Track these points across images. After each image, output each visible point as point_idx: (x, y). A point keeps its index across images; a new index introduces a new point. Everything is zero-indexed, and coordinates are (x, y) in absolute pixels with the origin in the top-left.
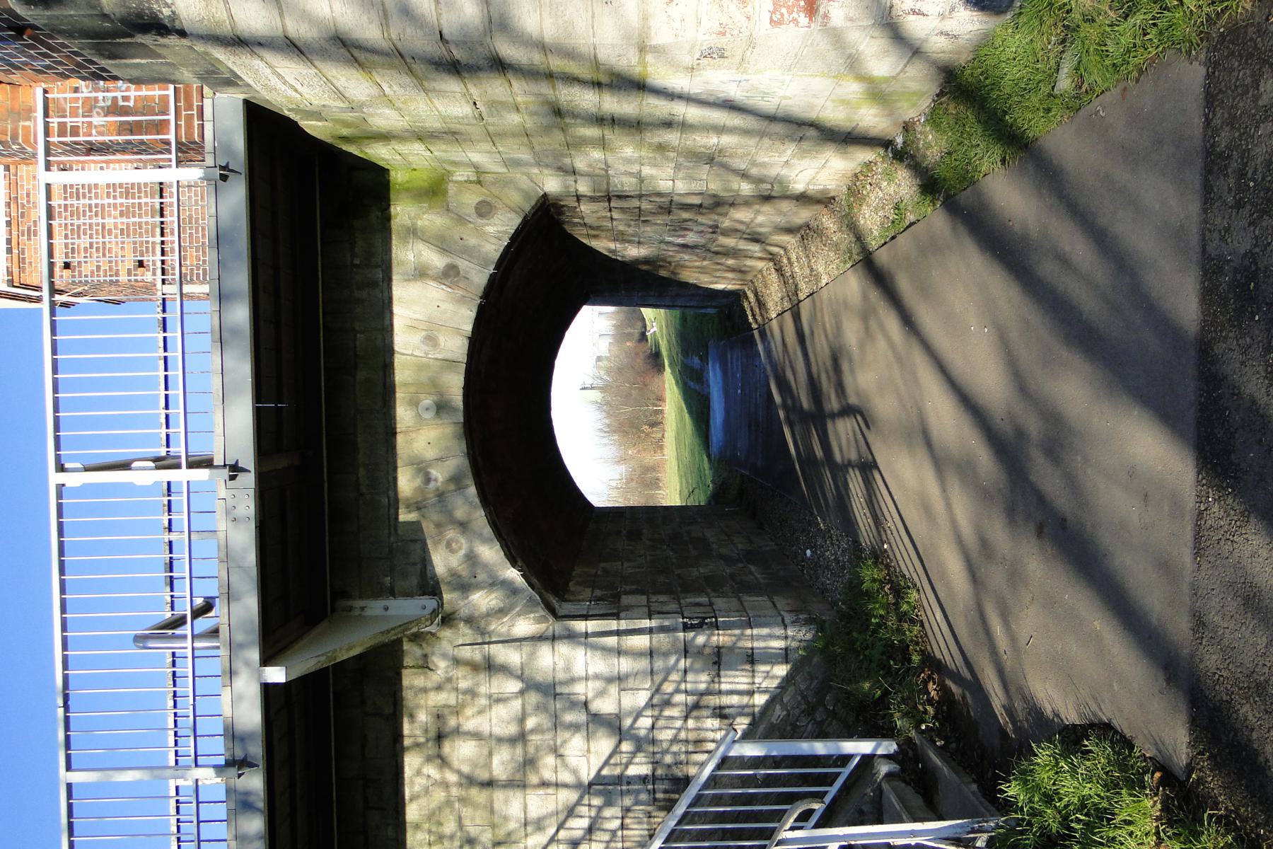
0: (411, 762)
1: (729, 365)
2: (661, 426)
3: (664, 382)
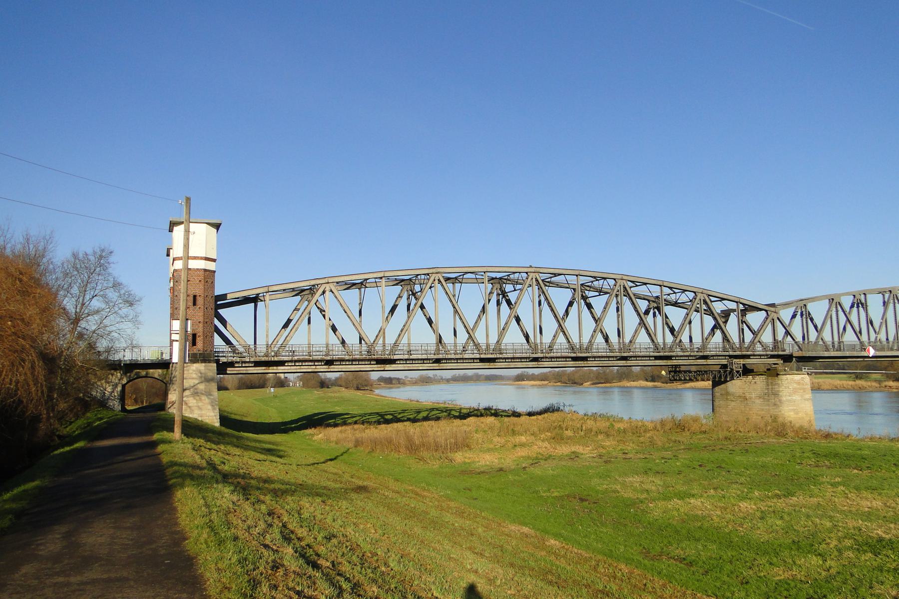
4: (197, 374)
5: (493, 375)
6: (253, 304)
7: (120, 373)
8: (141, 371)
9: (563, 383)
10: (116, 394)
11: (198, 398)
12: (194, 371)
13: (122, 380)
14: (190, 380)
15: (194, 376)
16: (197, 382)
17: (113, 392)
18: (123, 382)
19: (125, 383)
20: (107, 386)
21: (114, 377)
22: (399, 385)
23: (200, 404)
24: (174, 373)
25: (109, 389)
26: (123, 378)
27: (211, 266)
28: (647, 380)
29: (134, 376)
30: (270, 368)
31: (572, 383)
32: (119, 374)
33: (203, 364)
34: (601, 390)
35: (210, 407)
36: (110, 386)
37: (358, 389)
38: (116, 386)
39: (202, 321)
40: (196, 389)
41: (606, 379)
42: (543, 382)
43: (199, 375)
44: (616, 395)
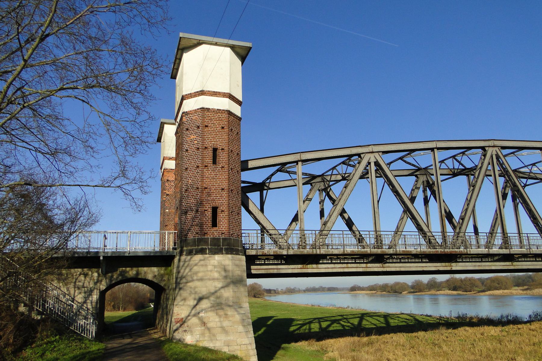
0: (80, 270)
1: (512, 180)
2: (113, 310)
3: (131, 311)
4: (219, 272)
5: (332, 287)
6: (259, 192)
7: (97, 272)
8: (128, 269)
9: (388, 292)
10: (89, 306)
11: (221, 312)
12: (215, 266)
13: (101, 284)
14: (209, 283)
15: (216, 275)
16: (219, 285)
17: (85, 302)
18: (101, 287)
19: (104, 288)
20: (76, 294)
21: (88, 279)
22: (275, 294)
23: (226, 324)
24: (182, 271)
25: (80, 298)
26: (101, 281)
27: (237, 110)
28: (450, 290)
29: (117, 278)
30: (309, 266)
31: (394, 292)
32: (96, 275)
33: (230, 256)
34: (416, 297)
35: (241, 328)
36: (80, 293)
37: (255, 297)
38: (90, 292)
39: (226, 188)
40: (218, 298)
41: (419, 289)
42: (372, 292)
43: (223, 273)
44: (427, 299)
